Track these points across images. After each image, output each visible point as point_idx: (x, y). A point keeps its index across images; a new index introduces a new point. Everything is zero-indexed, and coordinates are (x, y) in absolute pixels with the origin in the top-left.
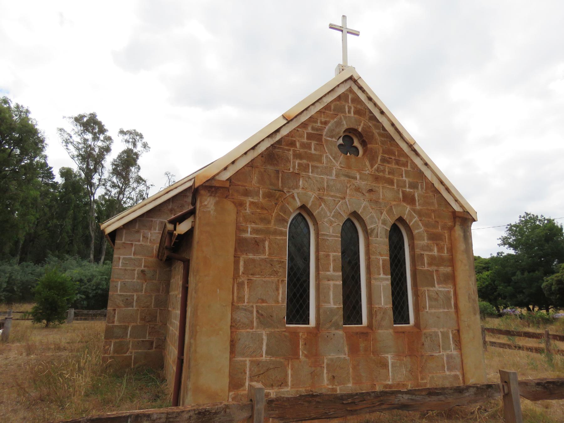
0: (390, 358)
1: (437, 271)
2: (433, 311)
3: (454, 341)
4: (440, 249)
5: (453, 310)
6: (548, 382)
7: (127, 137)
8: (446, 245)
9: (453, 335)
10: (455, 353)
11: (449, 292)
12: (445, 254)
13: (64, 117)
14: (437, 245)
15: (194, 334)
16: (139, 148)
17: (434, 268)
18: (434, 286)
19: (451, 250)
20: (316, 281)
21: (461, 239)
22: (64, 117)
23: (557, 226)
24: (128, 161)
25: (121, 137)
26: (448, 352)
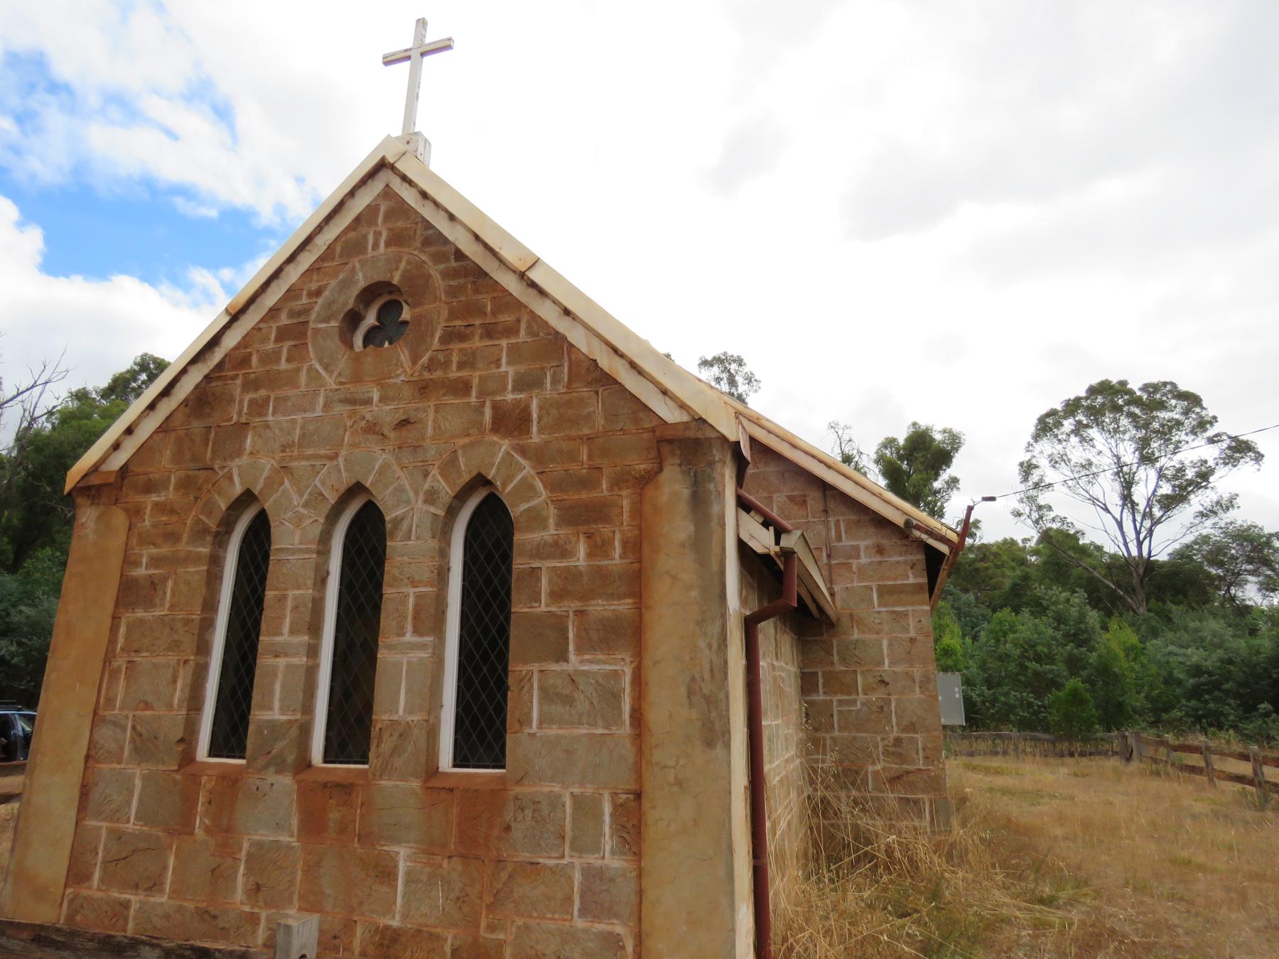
0: (403, 856)
5: (626, 729)
9: (618, 808)
10: (611, 859)
11: (616, 675)
12: (616, 559)
14: (589, 536)
17: (571, 606)
18: (562, 657)
19: (637, 547)
21: (683, 507)
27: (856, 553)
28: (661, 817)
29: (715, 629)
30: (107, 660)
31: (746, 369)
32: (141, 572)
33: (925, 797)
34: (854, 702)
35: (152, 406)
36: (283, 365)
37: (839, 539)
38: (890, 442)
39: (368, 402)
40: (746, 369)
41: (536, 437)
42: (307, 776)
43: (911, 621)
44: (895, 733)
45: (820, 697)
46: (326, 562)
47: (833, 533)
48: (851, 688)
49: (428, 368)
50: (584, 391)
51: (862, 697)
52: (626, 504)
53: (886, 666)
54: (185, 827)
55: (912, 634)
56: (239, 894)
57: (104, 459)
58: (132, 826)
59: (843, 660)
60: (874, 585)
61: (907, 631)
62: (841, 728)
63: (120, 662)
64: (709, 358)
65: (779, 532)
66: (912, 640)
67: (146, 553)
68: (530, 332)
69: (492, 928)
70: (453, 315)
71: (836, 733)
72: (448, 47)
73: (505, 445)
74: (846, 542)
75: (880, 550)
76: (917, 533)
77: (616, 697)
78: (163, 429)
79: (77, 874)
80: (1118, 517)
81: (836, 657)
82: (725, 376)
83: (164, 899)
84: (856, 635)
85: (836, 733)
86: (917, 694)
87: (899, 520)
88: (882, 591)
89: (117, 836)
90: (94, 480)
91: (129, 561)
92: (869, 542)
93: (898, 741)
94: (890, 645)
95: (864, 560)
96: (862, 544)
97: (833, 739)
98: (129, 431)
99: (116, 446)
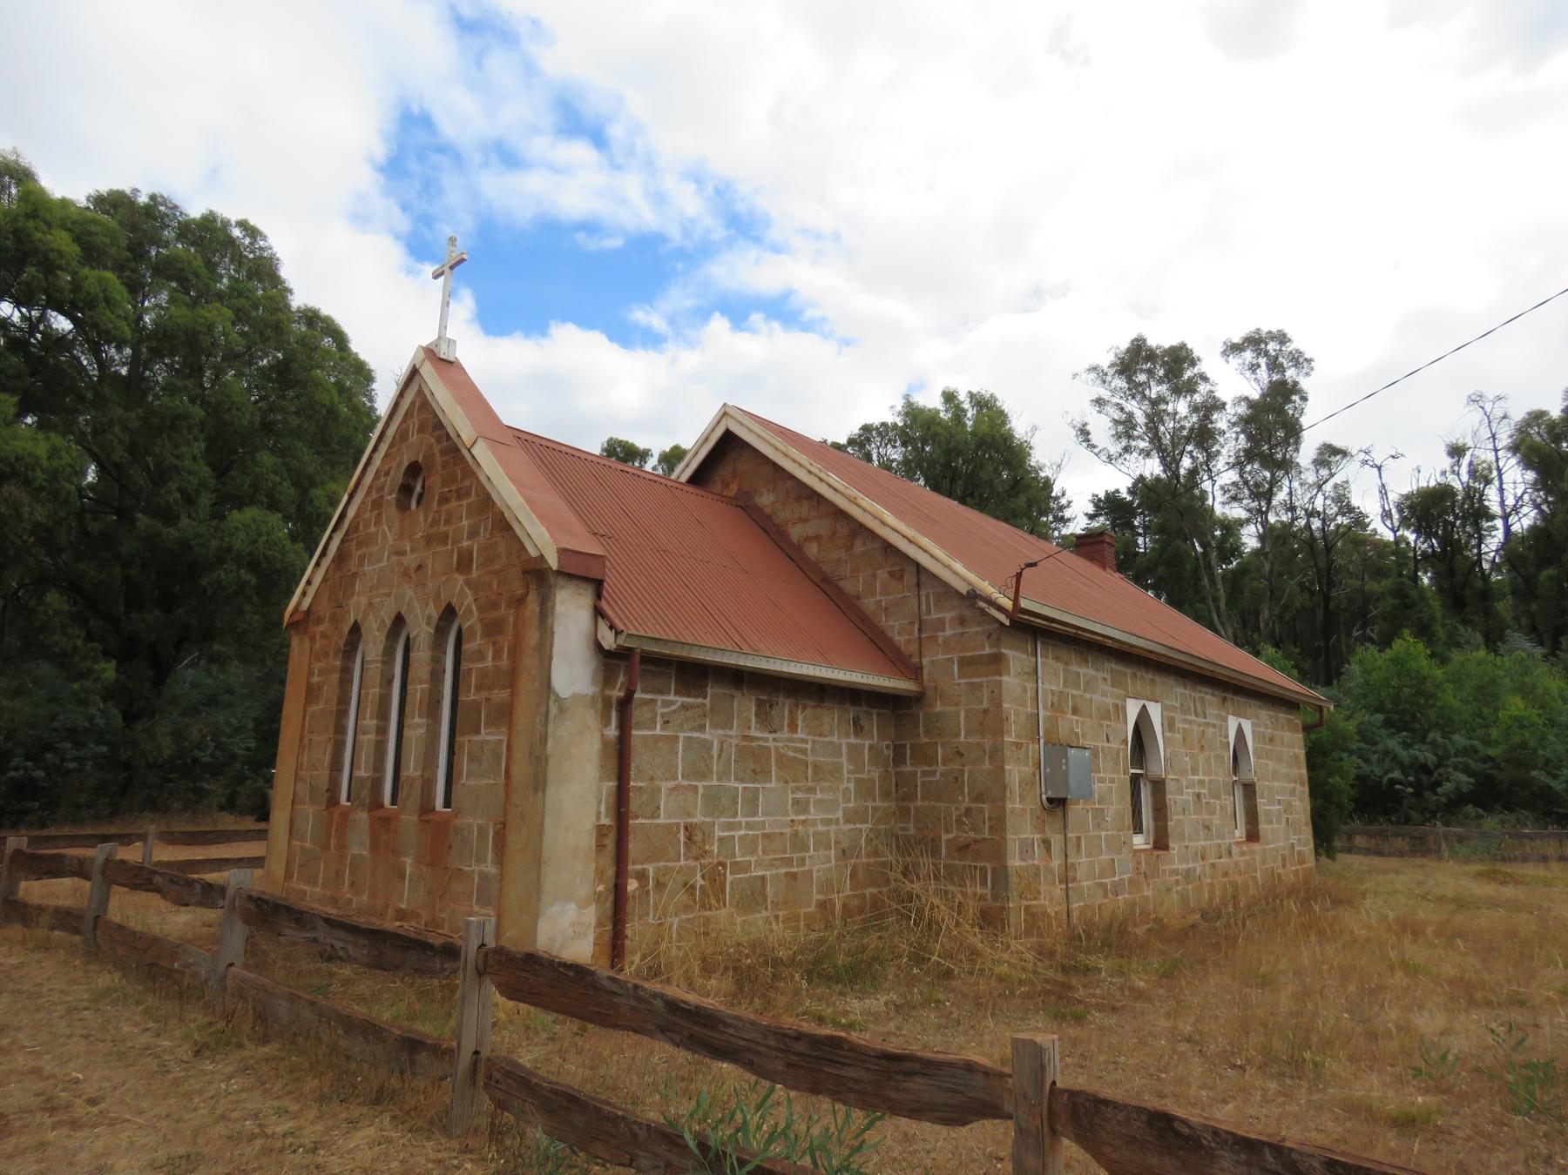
0: (409, 862)
1: (488, 699)
2: (472, 782)
3: (496, 846)
4: (497, 655)
5: (502, 781)
6: (565, 965)
7: (1248, 355)
8: (505, 642)
9: (496, 833)
10: (491, 869)
11: (500, 741)
12: (505, 662)
13: (1075, 376)
14: (494, 644)
15: (601, 831)
16: (1290, 374)
17: (484, 694)
18: (478, 732)
19: (515, 653)
20: (278, 730)
21: (535, 621)
22: (1075, 376)
23: (1158, 479)
24: (1272, 422)
25: (1235, 361)
26: (483, 867)
27: (941, 624)
28: (514, 840)
29: (543, 709)
30: (301, 740)
31: (1291, 347)
32: (315, 679)
33: (989, 866)
34: (933, 773)
35: (318, 564)
36: (373, 529)
37: (929, 612)
38: (1537, 417)
39: (404, 553)
40: (1291, 347)
41: (475, 574)
42: (379, 813)
43: (986, 693)
44: (966, 804)
45: (908, 768)
46: (392, 668)
47: (924, 607)
48: (932, 760)
49: (431, 526)
50: (498, 538)
51: (941, 768)
52: (511, 619)
53: (962, 738)
54: (326, 847)
55: (985, 705)
56: (346, 887)
57: (299, 603)
58: (308, 845)
59: (928, 733)
60: (955, 657)
61: (981, 702)
62: (924, 798)
63: (306, 741)
64: (1237, 340)
65: (618, 633)
66: (985, 711)
67: (318, 666)
68: (477, 495)
69: (441, 910)
70: (443, 486)
71: (919, 803)
72: (463, 260)
73: (461, 579)
74: (935, 616)
75: (962, 621)
76: (982, 604)
77: (500, 758)
78: (324, 580)
79: (288, 875)
80: (601, 621)
81: (921, 730)
82: (1263, 361)
83: (318, 890)
84: (939, 708)
85: (919, 803)
86: (987, 766)
87: (964, 589)
88: (963, 663)
89: (303, 849)
90: (295, 618)
91: (310, 673)
92: (953, 614)
93: (968, 812)
94: (966, 717)
95: (949, 632)
96: (948, 616)
97: (917, 809)
98: (309, 582)
99: (304, 594)
